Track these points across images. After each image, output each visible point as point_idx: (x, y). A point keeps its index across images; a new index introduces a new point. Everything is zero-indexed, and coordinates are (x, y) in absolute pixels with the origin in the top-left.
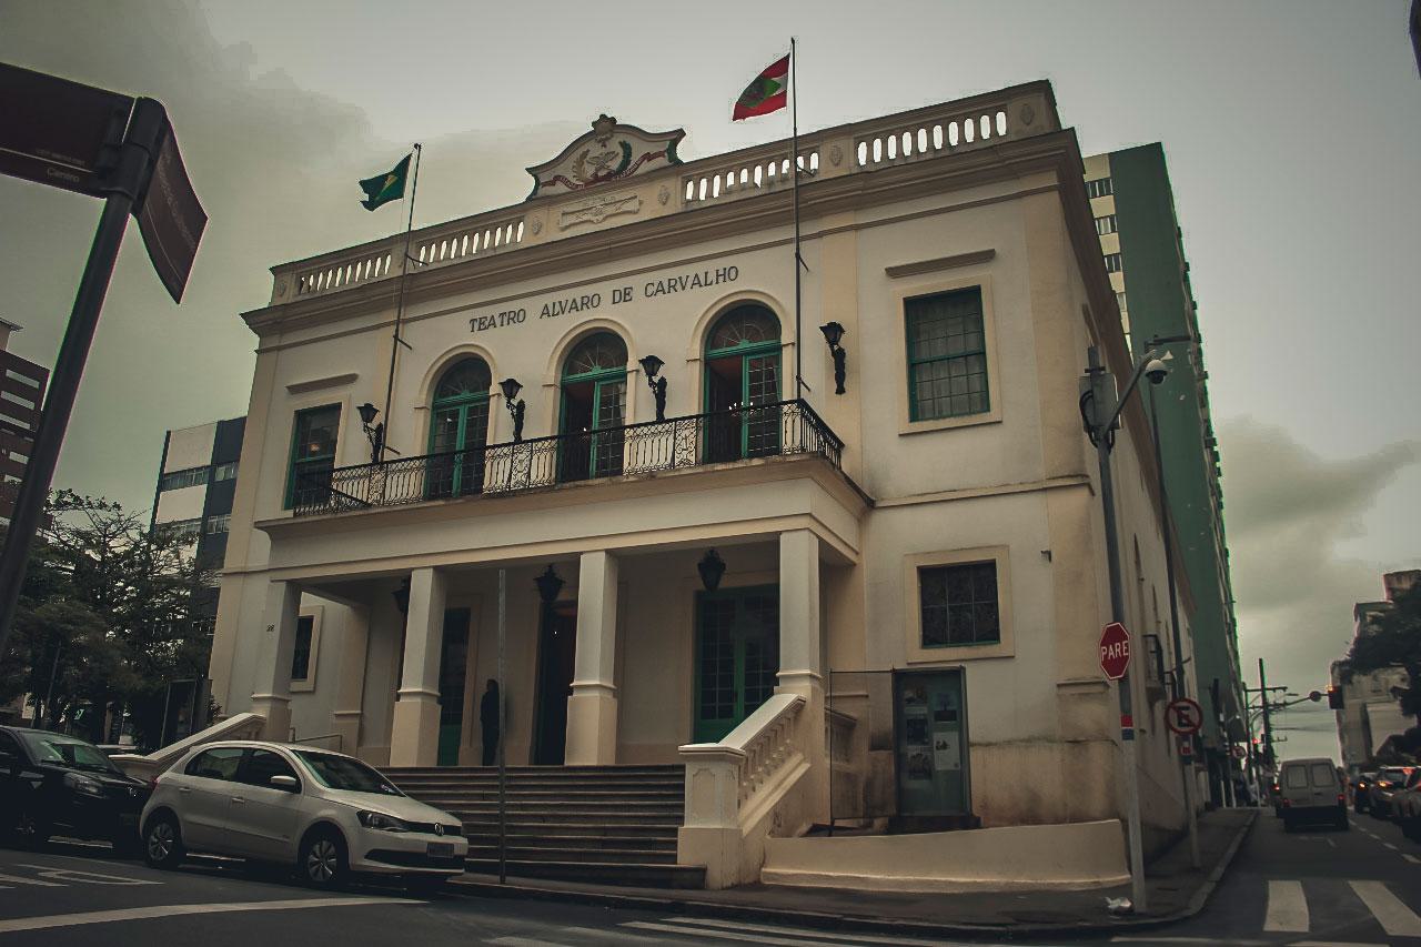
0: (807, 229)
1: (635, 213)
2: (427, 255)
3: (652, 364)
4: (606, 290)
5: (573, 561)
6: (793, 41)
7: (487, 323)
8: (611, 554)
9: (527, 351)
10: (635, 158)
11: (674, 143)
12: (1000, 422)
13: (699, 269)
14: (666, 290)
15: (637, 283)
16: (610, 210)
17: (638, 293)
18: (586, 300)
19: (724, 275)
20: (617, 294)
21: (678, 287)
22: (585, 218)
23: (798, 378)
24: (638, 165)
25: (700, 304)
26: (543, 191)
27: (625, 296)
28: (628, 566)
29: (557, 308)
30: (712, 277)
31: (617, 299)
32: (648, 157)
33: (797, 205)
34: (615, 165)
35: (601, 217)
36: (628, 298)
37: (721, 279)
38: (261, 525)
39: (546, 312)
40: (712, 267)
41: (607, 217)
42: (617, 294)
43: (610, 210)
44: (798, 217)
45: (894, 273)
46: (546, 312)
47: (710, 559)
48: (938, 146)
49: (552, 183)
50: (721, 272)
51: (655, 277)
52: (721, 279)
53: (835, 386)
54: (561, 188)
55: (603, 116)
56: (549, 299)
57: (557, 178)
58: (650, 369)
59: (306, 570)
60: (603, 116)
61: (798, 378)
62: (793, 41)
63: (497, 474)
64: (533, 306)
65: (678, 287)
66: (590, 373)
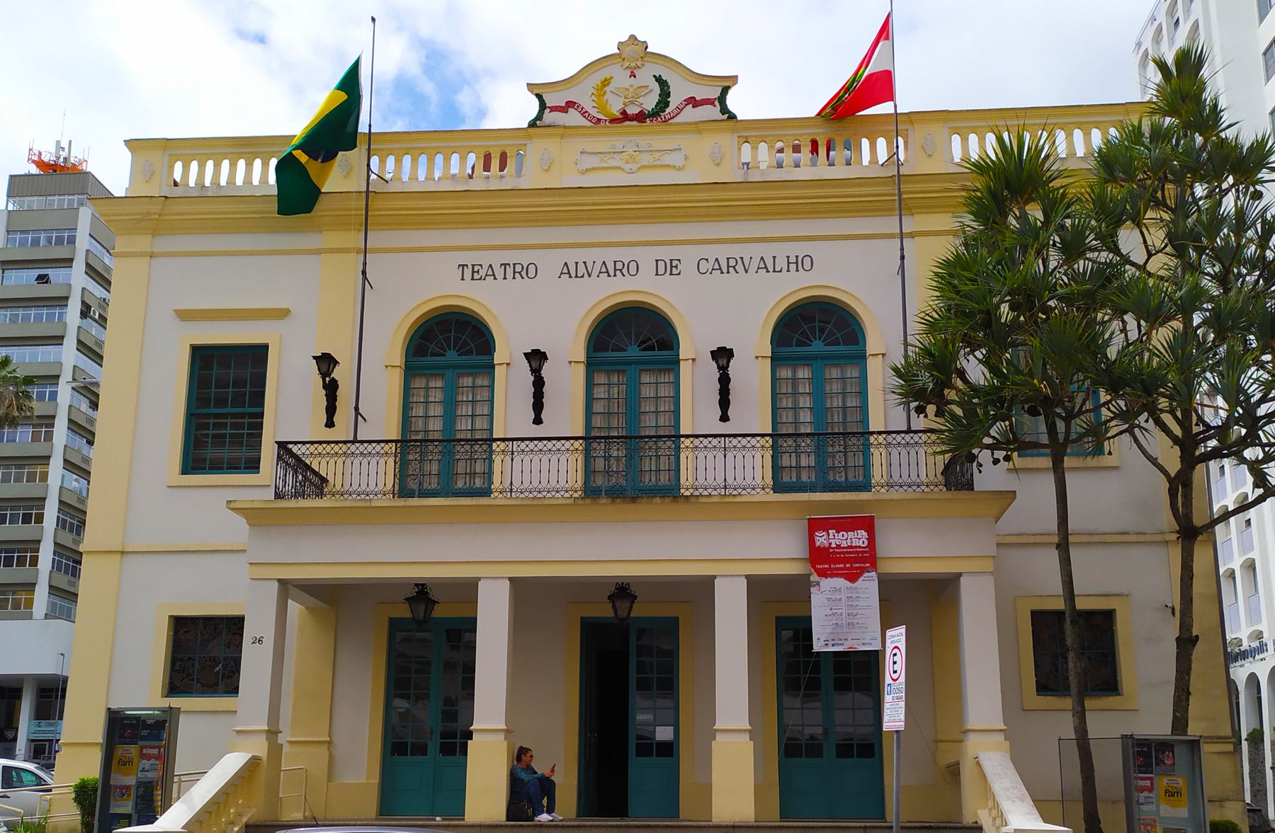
0: (910, 224)
1: (680, 169)
2: (191, 174)
3: (722, 355)
4: (646, 257)
5: (705, 587)
6: (373, 20)
7: (482, 273)
8: (517, 584)
9: (542, 314)
10: (675, 101)
11: (725, 90)
12: (1116, 468)
13: (767, 251)
14: (612, 273)
15: (689, 256)
16: (646, 159)
17: (687, 267)
18: (619, 266)
19: (797, 263)
20: (661, 264)
21: (740, 267)
22: (612, 163)
23: (357, 409)
24: (680, 110)
25: (774, 295)
26: (549, 117)
27: (672, 267)
28: (529, 595)
29: (582, 270)
30: (782, 263)
31: (661, 271)
32: (693, 102)
33: (900, 195)
34: (650, 103)
35: (634, 167)
36: (675, 271)
37: (793, 267)
38: (232, 505)
39: (566, 271)
40: (783, 251)
41: (642, 167)
42: (661, 264)
43: (646, 159)
44: (903, 208)
45: (185, 315)
46: (566, 271)
47: (422, 593)
48: (223, 182)
49: (564, 109)
50: (793, 260)
51: (712, 252)
52: (793, 267)
53: (323, 418)
54: (573, 117)
55: (633, 37)
56: (572, 256)
57: (571, 104)
58: (324, 369)
59: (417, 567)
60: (633, 37)
61: (357, 409)
62: (373, 20)
63: (507, 471)
64: (550, 262)
65: (740, 267)
66: (808, 349)
